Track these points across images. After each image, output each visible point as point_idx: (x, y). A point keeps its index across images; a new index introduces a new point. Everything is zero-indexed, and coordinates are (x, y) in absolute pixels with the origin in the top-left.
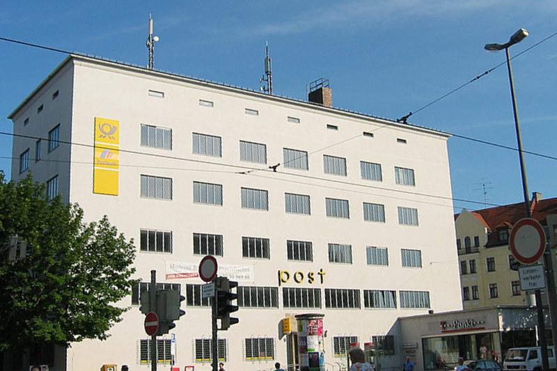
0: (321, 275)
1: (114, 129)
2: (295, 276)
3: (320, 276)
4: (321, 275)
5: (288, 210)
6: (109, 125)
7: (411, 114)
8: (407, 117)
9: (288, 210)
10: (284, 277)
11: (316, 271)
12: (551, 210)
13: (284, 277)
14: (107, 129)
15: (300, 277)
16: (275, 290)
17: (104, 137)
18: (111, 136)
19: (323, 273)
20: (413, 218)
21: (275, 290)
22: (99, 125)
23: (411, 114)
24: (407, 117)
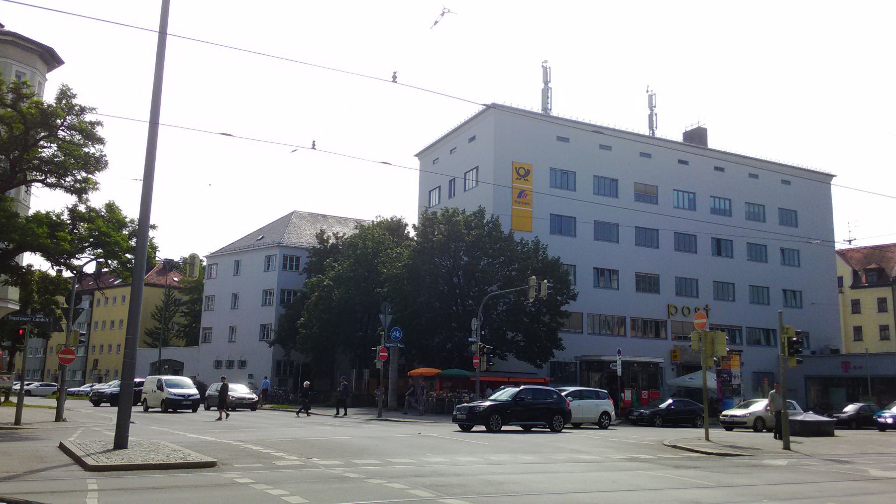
0: (707, 310)
1: (528, 172)
2: (689, 313)
3: (705, 311)
4: (707, 310)
5: (638, 244)
6: (525, 169)
7: (855, 239)
8: (852, 240)
9: (638, 244)
10: (673, 310)
11: (702, 306)
12: (707, 470)
13: (673, 310)
14: (522, 172)
15: (675, 311)
16: (664, 323)
17: (520, 179)
18: (525, 178)
19: (708, 309)
20: (764, 258)
21: (664, 323)
22: (516, 168)
23: (855, 239)
24: (852, 240)
